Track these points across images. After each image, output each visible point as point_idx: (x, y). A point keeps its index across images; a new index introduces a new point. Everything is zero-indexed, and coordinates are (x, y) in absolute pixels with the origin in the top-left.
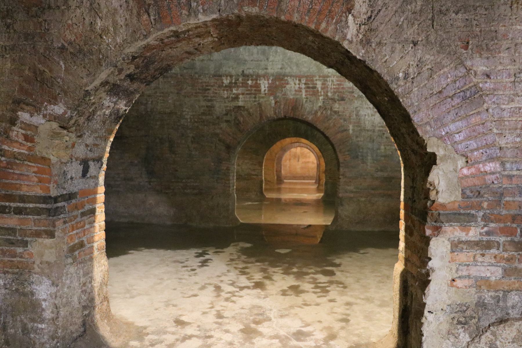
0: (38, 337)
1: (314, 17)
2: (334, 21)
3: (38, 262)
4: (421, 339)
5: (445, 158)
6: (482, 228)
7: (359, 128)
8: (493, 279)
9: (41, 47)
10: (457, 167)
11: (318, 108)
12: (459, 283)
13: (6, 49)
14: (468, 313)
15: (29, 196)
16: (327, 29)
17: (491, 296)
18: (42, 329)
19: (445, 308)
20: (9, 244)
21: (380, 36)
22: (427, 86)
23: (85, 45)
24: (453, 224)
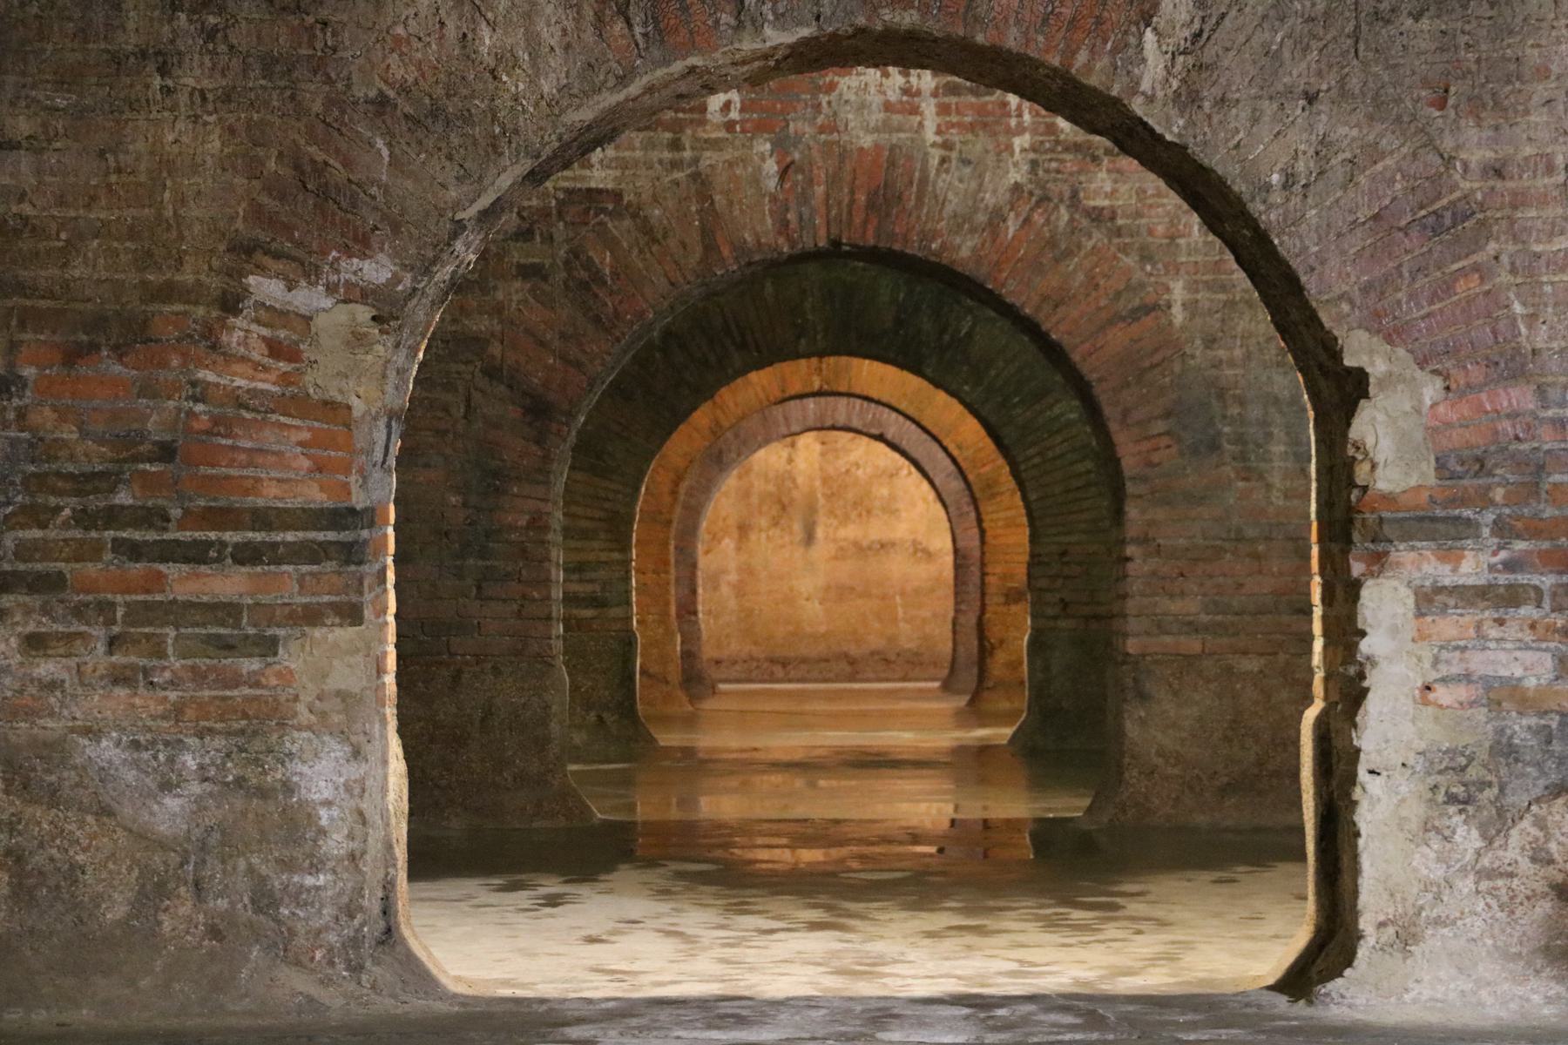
0: (302, 914)
1: (1060, 35)
2: (1109, 46)
3: (307, 698)
4: (1356, 846)
5: (1388, 381)
6: (1495, 554)
7: (1222, 297)
8: (1531, 682)
9: (314, 96)
10: (1420, 401)
11: (1003, 196)
12: (1442, 694)
13: (204, 99)
14: (1473, 773)
15: (286, 510)
16: (1093, 68)
17: (1529, 728)
18: (318, 888)
19: (1411, 762)
20: (219, 648)
21: (1223, 80)
22: (1342, 202)
23: (448, 96)
24: (1419, 544)
